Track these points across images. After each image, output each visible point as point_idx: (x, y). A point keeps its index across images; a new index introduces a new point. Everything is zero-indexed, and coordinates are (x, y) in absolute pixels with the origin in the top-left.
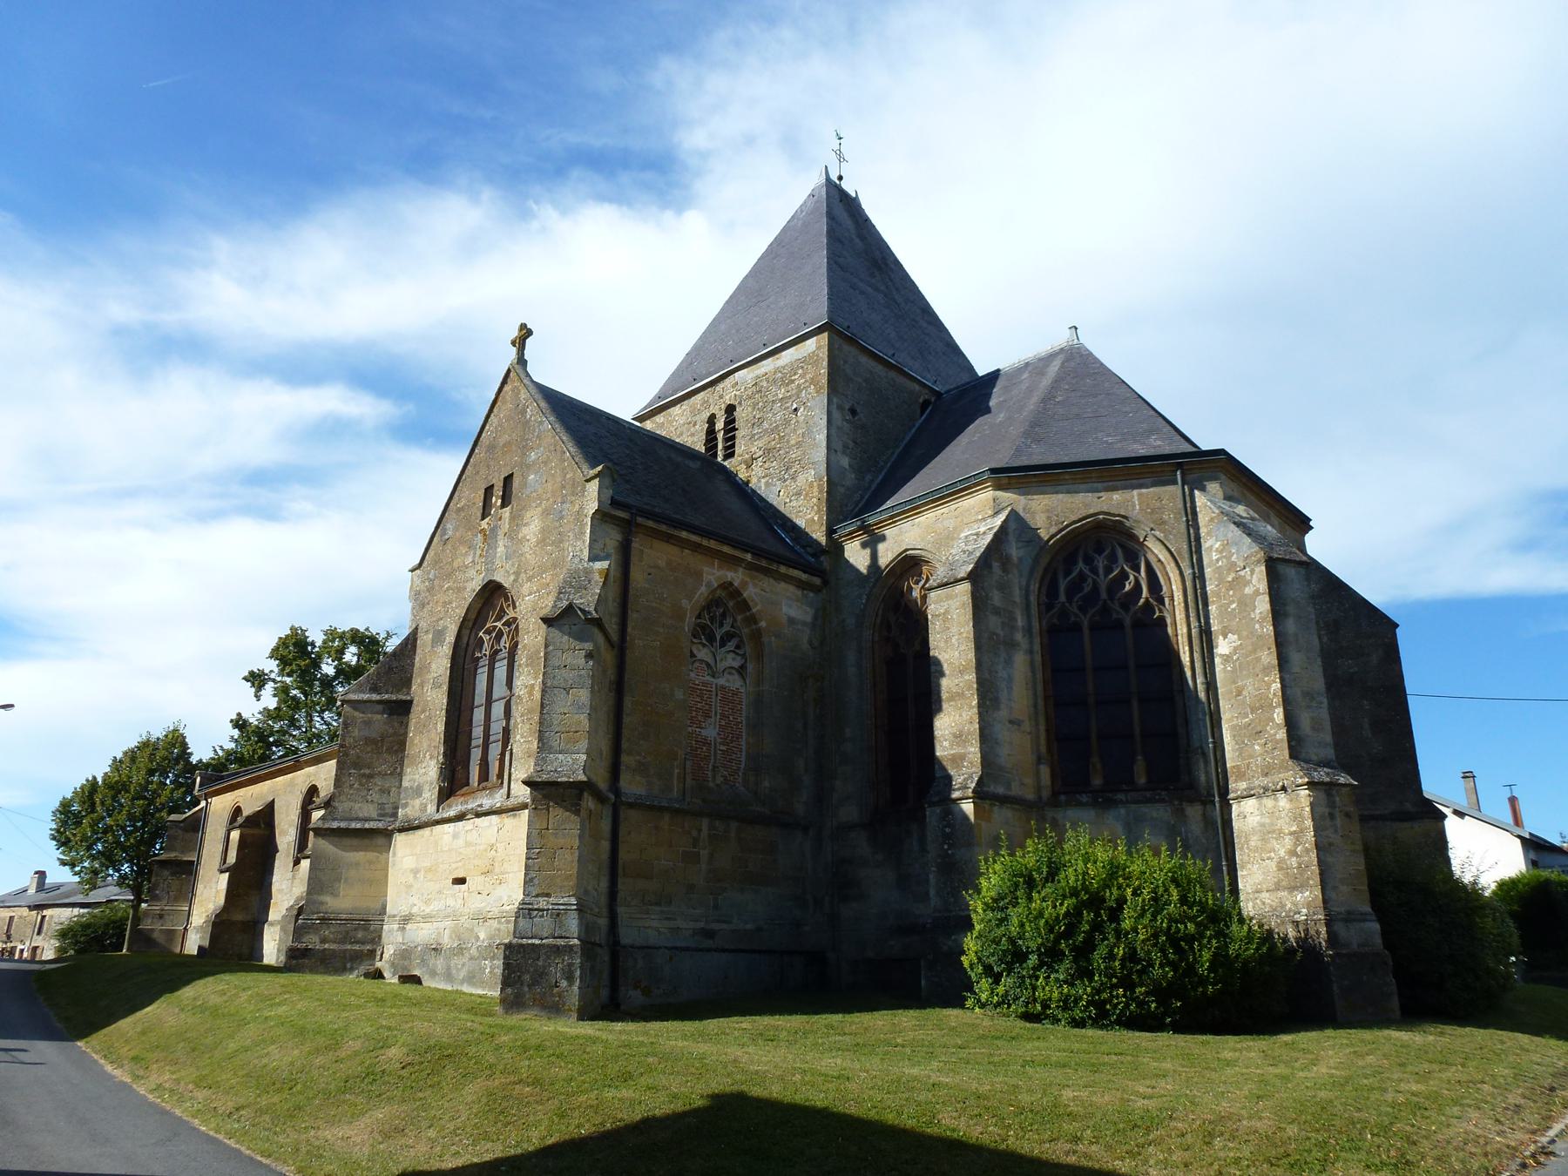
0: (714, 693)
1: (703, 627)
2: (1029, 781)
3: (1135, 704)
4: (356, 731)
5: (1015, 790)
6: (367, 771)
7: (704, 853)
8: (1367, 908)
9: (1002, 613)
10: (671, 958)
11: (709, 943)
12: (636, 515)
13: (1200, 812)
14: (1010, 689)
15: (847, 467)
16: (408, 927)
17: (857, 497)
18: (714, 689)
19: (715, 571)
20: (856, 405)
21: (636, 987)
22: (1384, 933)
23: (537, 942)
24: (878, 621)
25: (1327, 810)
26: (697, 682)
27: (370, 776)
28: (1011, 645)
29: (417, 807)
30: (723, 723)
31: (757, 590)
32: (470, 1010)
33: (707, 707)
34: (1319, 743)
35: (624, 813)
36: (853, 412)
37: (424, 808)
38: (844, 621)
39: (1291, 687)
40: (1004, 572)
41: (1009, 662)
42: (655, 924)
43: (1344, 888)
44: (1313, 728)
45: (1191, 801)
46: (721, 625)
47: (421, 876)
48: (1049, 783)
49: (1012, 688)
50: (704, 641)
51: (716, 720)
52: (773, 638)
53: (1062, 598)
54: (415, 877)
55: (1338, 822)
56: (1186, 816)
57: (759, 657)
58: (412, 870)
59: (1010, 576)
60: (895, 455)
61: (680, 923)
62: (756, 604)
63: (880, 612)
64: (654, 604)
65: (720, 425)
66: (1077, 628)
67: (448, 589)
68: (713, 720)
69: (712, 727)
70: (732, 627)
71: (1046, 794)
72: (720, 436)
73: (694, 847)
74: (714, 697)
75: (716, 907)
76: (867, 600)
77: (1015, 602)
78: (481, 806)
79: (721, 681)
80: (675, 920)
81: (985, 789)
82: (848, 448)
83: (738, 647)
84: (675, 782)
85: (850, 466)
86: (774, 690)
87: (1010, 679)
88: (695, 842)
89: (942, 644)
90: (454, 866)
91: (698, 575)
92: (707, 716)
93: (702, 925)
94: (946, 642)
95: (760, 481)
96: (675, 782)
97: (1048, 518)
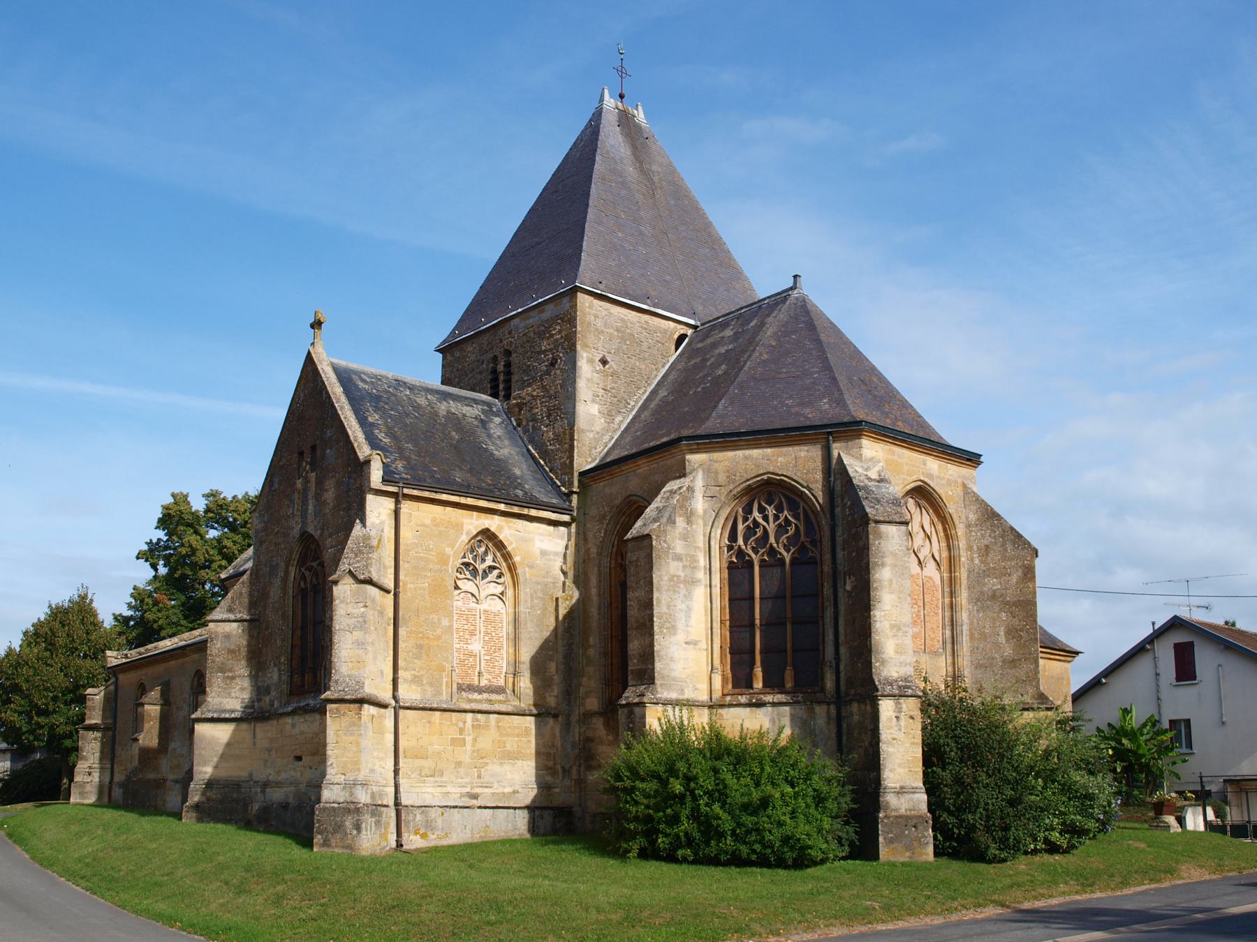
0: (478, 616)
1: (467, 565)
2: (704, 686)
3: (789, 626)
4: (219, 643)
5: (689, 694)
6: (230, 674)
7: (469, 739)
8: (919, 784)
9: (684, 559)
10: (443, 814)
11: (474, 802)
12: (403, 487)
13: (826, 711)
14: (688, 617)
15: (597, 413)
16: (268, 790)
17: (606, 438)
18: (478, 614)
19: (474, 521)
20: (606, 355)
21: (416, 833)
22: (930, 805)
23: (336, 805)
24: (615, 550)
25: (895, 714)
26: (463, 609)
27: (233, 678)
28: (693, 582)
29: (268, 702)
30: (487, 638)
31: (513, 532)
32: (426, 852)
33: (472, 628)
34: (901, 663)
35: (402, 713)
36: (604, 362)
37: (272, 704)
38: (589, 549)
39: (881, 622)
40: (688, 524)
41: (688, 596)
42: (430, 790)
43: (901, 770)
44: (896, 652)
45: (820, 703)
46: (483, 560)
47: (273, 753)
48: (720, 688)
49: (690, 617)
50: (469, 577)
51: (480, 638)
52: (527, 569)
53: (740, 541)
54: (270, 755)
55: (902, 723)
56: (815, 713)
57: (515, 584)
58: (267, 749)
59: (694, 526)
60: (647, 394)
61: (449, 789)
62: (512, 543)
63: (616, 543)
64: (421, 555)
65: (501, 367)
66: (750, 564)
67: (278, 532)
68: (477, 637)
69: (477, 642)
70: (494, 561)
71: (717, 694)
72: (501, 377)
73: (461, 735)
74: (478, 619)
75: (479, 777)
76: (605, 533)
77: (698, 547)
78: (308, 705)
79: (484, 606)
80: (445, 786)
81: (659, 696)
82: (598, 396)
83: (499, 577)
84: (444, 688)
85: (599, 412)
86: (528, 610)
87: (689, 609)
88: (461, 731)
89: (634, 585)
90: (294, 747)
91: (459, 527)
92: (472, 634)
93: (468, 790)
94: (637, 583)
95: (528, 425)
96: (444, 688)
97: (728, 477)
